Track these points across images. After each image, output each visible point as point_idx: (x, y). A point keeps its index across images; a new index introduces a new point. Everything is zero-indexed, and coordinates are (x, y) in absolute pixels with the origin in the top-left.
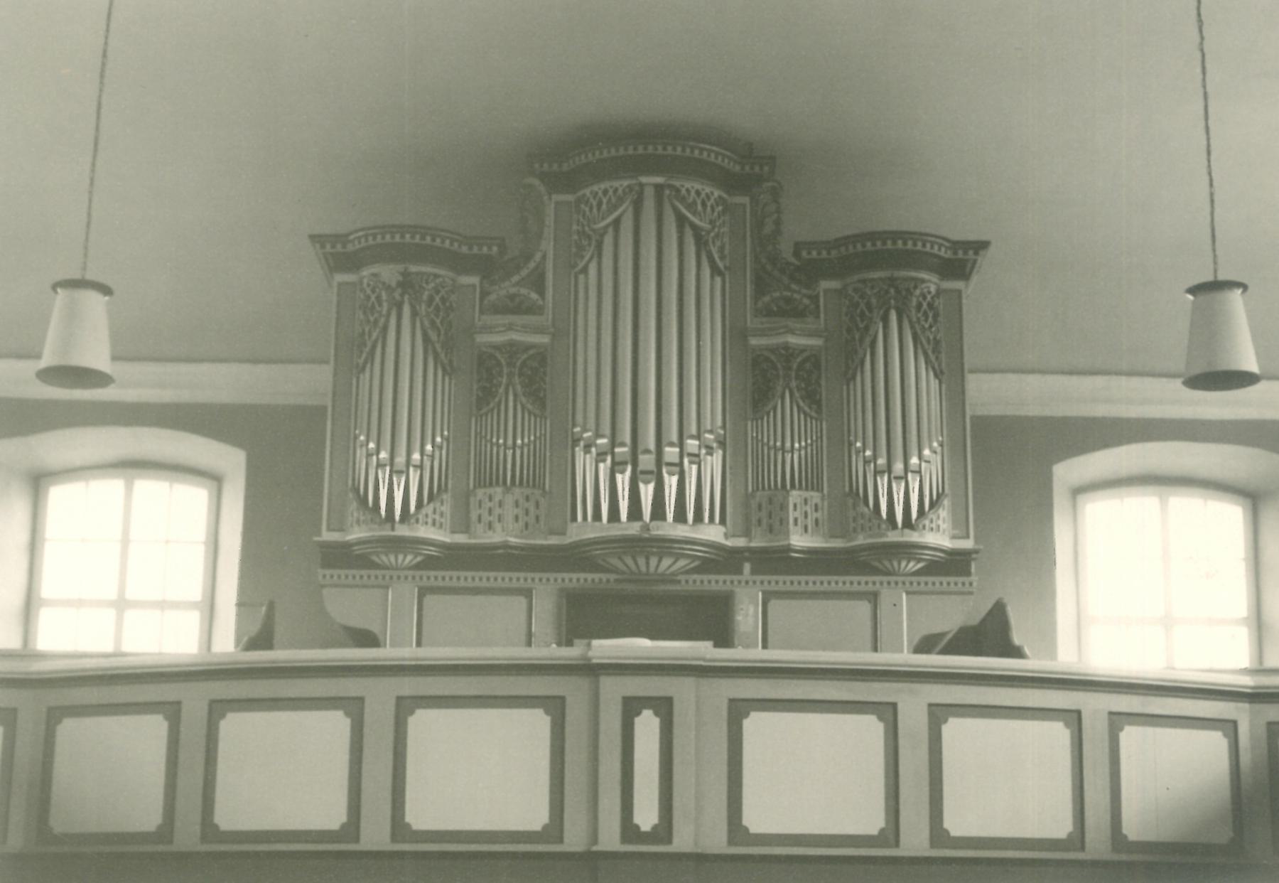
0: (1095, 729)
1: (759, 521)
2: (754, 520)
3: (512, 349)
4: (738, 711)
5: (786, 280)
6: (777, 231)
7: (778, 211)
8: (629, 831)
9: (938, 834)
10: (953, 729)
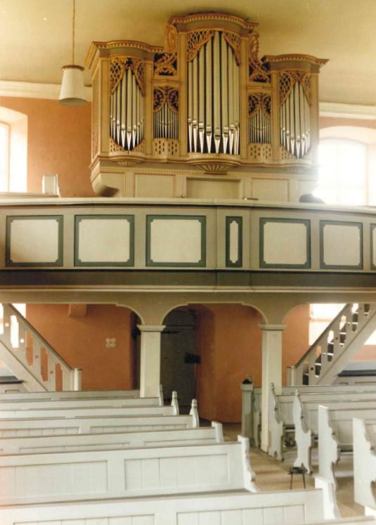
0: (315, 226)
1: (251, 154)
2: (249, 154)
3: (167, 89)
4: (263, 221)
5: (260, 69)
6: (257, 51)
7: (257, 43)
8: (228, 262)
9: (322, 265)
10: (84, 224)
